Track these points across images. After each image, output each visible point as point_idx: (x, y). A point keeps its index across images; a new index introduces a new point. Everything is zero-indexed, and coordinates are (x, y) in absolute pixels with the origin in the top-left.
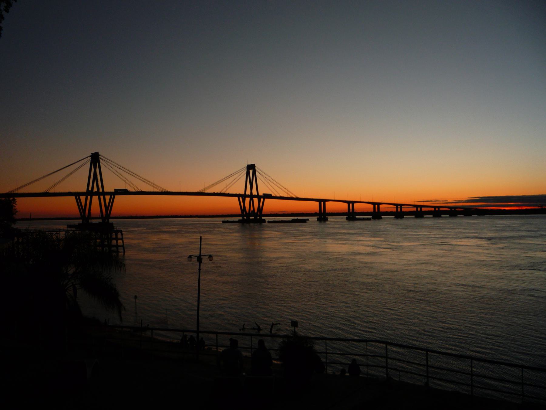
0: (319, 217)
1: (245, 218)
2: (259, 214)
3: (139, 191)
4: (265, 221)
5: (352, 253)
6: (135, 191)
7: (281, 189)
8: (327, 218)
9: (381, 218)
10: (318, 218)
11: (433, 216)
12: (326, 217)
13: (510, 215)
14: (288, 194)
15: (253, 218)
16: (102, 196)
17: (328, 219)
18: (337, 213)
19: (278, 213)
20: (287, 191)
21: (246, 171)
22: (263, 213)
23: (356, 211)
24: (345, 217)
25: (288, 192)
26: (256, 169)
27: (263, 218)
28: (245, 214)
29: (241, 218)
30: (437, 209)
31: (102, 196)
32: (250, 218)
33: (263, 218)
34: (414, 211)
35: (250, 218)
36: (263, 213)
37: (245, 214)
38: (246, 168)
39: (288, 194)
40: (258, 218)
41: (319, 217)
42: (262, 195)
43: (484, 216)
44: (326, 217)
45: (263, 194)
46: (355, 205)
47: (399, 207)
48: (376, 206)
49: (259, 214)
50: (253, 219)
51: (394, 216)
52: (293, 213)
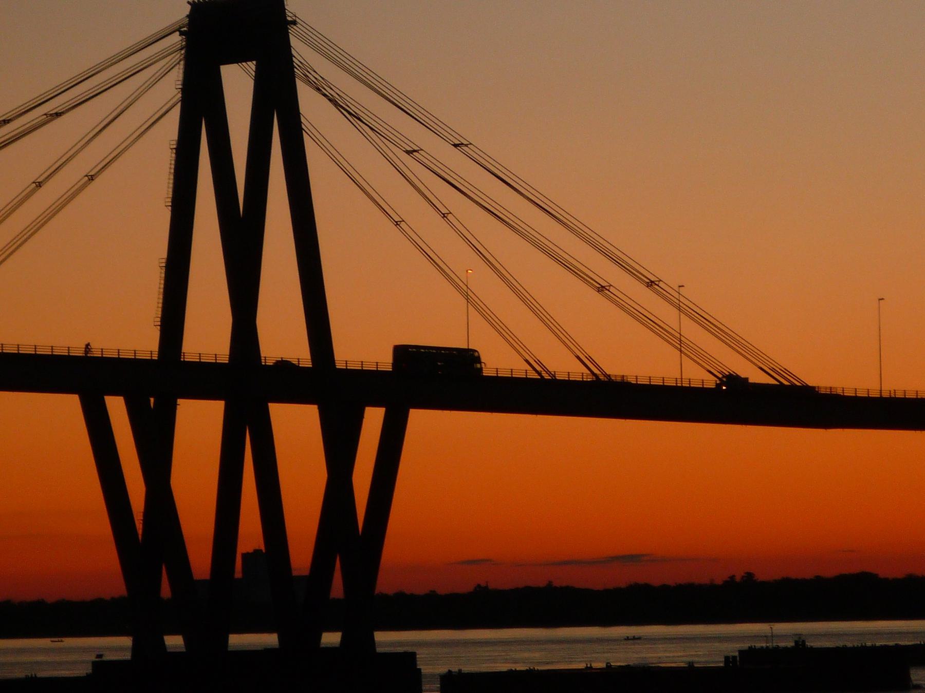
1: (174, 642)
2: (337, 589)
3: (757, 377)
6: (710, 382)
7: (601, 289)
9: (739, 651)
14: (680, 344)
15: (271, 640)
17: (723, 660)
19: (562, 579)
20: (667, 314)
21: (177, 76)
22: (386, 584)
25: (693, 332)
26: (299, 48)
28: (166, 591)
29: (126, 641)
32: (237, 640)
35: (237, 640)
36: (386, 584)
37: (166, 591)
38: (176, 38)
39: (680, 344)
40: (331, 639)
42: (384, 360)
43: (745, 646)
45: (402, 353)
49: (337, 589)
50: (267, 653)
52: (749, 577)
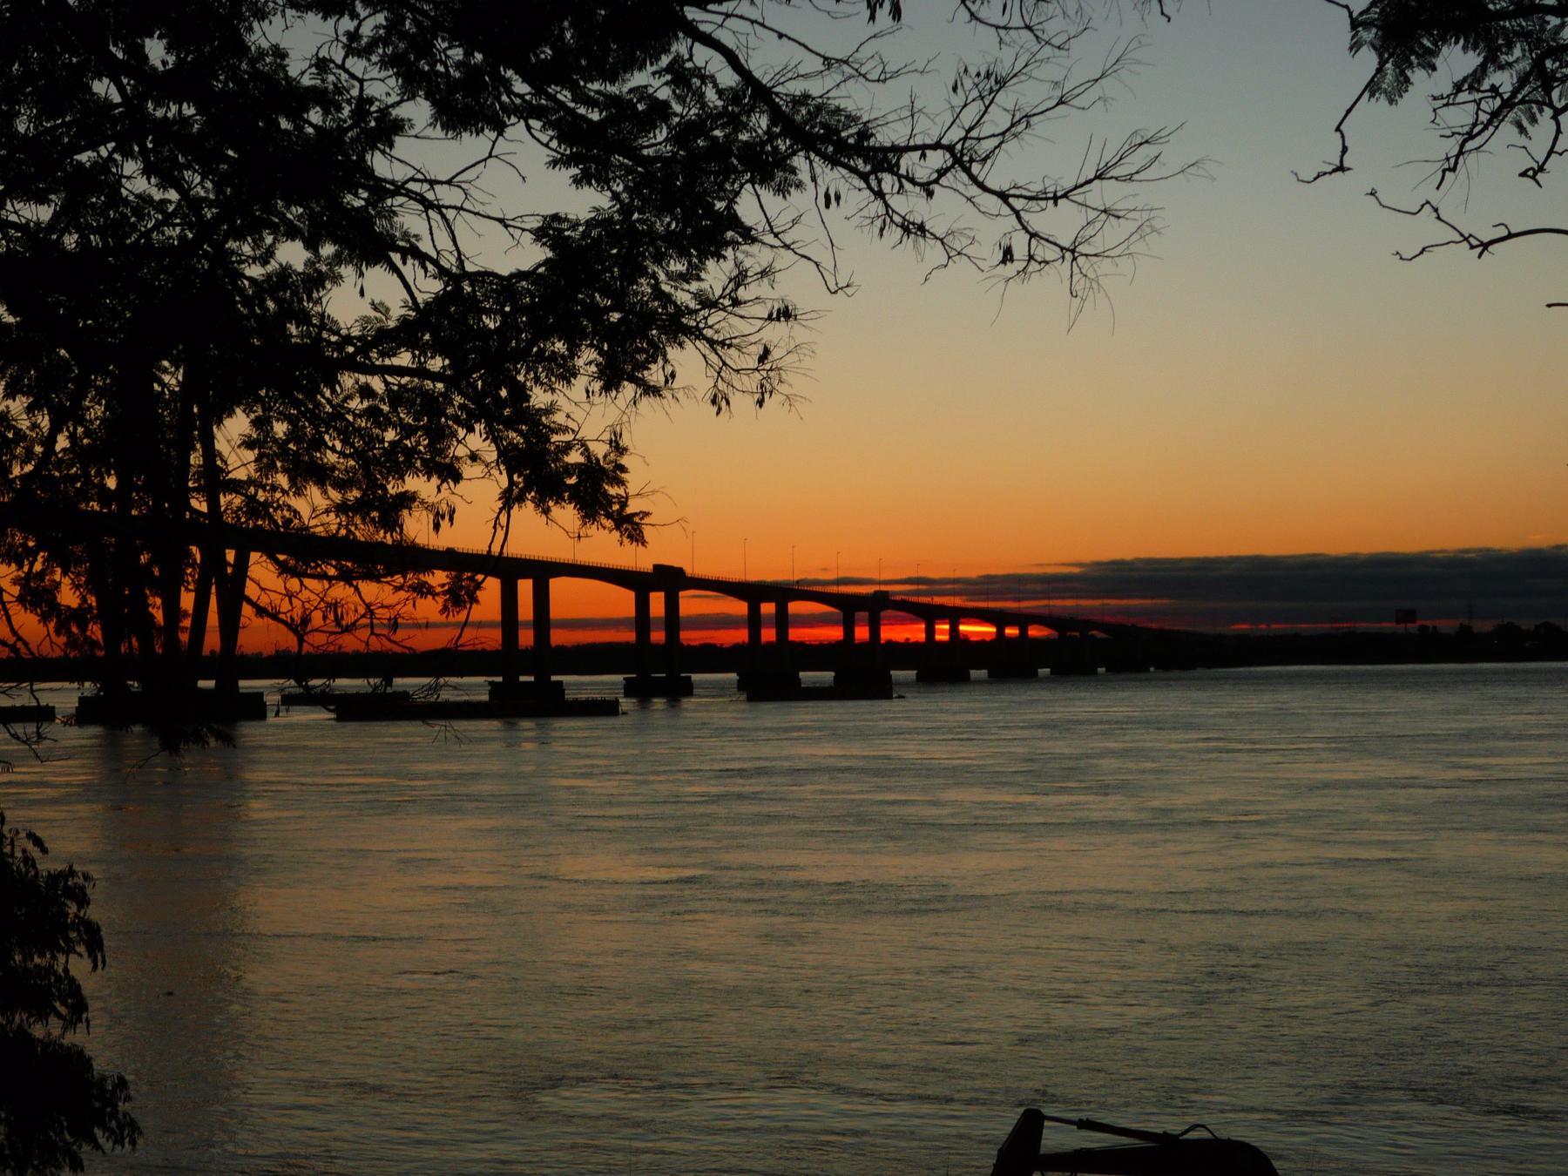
0: (499, 679)
4: (264, 704)
5: (752, 814)
8: (561, 683)
10: (491, 683)
11: (990, 675)
12: (554, 678)
13: (1305, 668)
16: (662, 595)
18: (588, 644)
23: (557, 643)
24: (619, 678)
27: (245, 685)
30: (1011, 631)
31: (662, 595)
32: (532, 679)
33: (245, 685)
34: (736, 648)
35: (532, 679)
40: (207, 684)
41: (499, 679)
44: (554, 678)
46: (559, 586)
47: (768, 608)
48: (525, 587)
50: (555, 674)
51: (733, 676)
